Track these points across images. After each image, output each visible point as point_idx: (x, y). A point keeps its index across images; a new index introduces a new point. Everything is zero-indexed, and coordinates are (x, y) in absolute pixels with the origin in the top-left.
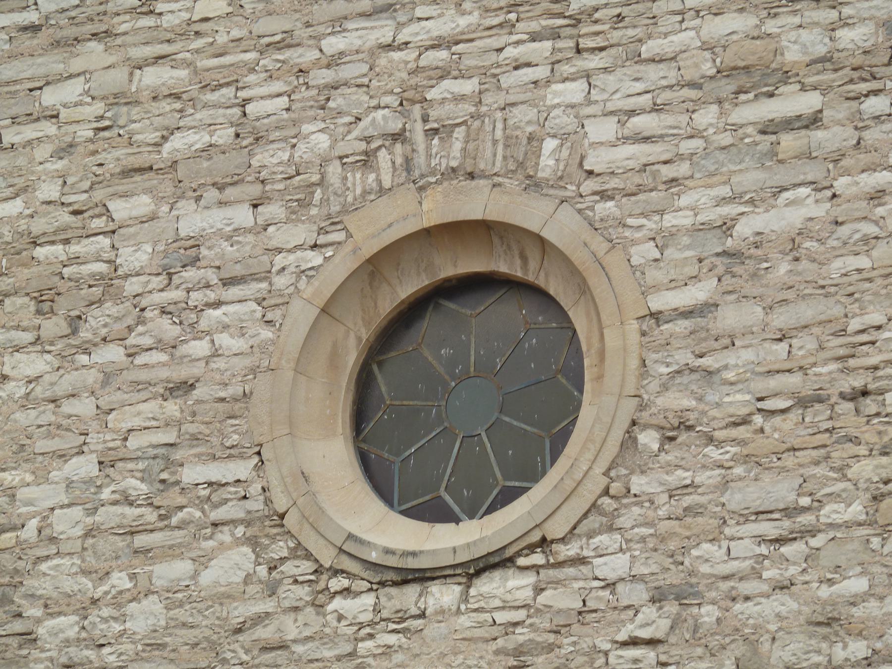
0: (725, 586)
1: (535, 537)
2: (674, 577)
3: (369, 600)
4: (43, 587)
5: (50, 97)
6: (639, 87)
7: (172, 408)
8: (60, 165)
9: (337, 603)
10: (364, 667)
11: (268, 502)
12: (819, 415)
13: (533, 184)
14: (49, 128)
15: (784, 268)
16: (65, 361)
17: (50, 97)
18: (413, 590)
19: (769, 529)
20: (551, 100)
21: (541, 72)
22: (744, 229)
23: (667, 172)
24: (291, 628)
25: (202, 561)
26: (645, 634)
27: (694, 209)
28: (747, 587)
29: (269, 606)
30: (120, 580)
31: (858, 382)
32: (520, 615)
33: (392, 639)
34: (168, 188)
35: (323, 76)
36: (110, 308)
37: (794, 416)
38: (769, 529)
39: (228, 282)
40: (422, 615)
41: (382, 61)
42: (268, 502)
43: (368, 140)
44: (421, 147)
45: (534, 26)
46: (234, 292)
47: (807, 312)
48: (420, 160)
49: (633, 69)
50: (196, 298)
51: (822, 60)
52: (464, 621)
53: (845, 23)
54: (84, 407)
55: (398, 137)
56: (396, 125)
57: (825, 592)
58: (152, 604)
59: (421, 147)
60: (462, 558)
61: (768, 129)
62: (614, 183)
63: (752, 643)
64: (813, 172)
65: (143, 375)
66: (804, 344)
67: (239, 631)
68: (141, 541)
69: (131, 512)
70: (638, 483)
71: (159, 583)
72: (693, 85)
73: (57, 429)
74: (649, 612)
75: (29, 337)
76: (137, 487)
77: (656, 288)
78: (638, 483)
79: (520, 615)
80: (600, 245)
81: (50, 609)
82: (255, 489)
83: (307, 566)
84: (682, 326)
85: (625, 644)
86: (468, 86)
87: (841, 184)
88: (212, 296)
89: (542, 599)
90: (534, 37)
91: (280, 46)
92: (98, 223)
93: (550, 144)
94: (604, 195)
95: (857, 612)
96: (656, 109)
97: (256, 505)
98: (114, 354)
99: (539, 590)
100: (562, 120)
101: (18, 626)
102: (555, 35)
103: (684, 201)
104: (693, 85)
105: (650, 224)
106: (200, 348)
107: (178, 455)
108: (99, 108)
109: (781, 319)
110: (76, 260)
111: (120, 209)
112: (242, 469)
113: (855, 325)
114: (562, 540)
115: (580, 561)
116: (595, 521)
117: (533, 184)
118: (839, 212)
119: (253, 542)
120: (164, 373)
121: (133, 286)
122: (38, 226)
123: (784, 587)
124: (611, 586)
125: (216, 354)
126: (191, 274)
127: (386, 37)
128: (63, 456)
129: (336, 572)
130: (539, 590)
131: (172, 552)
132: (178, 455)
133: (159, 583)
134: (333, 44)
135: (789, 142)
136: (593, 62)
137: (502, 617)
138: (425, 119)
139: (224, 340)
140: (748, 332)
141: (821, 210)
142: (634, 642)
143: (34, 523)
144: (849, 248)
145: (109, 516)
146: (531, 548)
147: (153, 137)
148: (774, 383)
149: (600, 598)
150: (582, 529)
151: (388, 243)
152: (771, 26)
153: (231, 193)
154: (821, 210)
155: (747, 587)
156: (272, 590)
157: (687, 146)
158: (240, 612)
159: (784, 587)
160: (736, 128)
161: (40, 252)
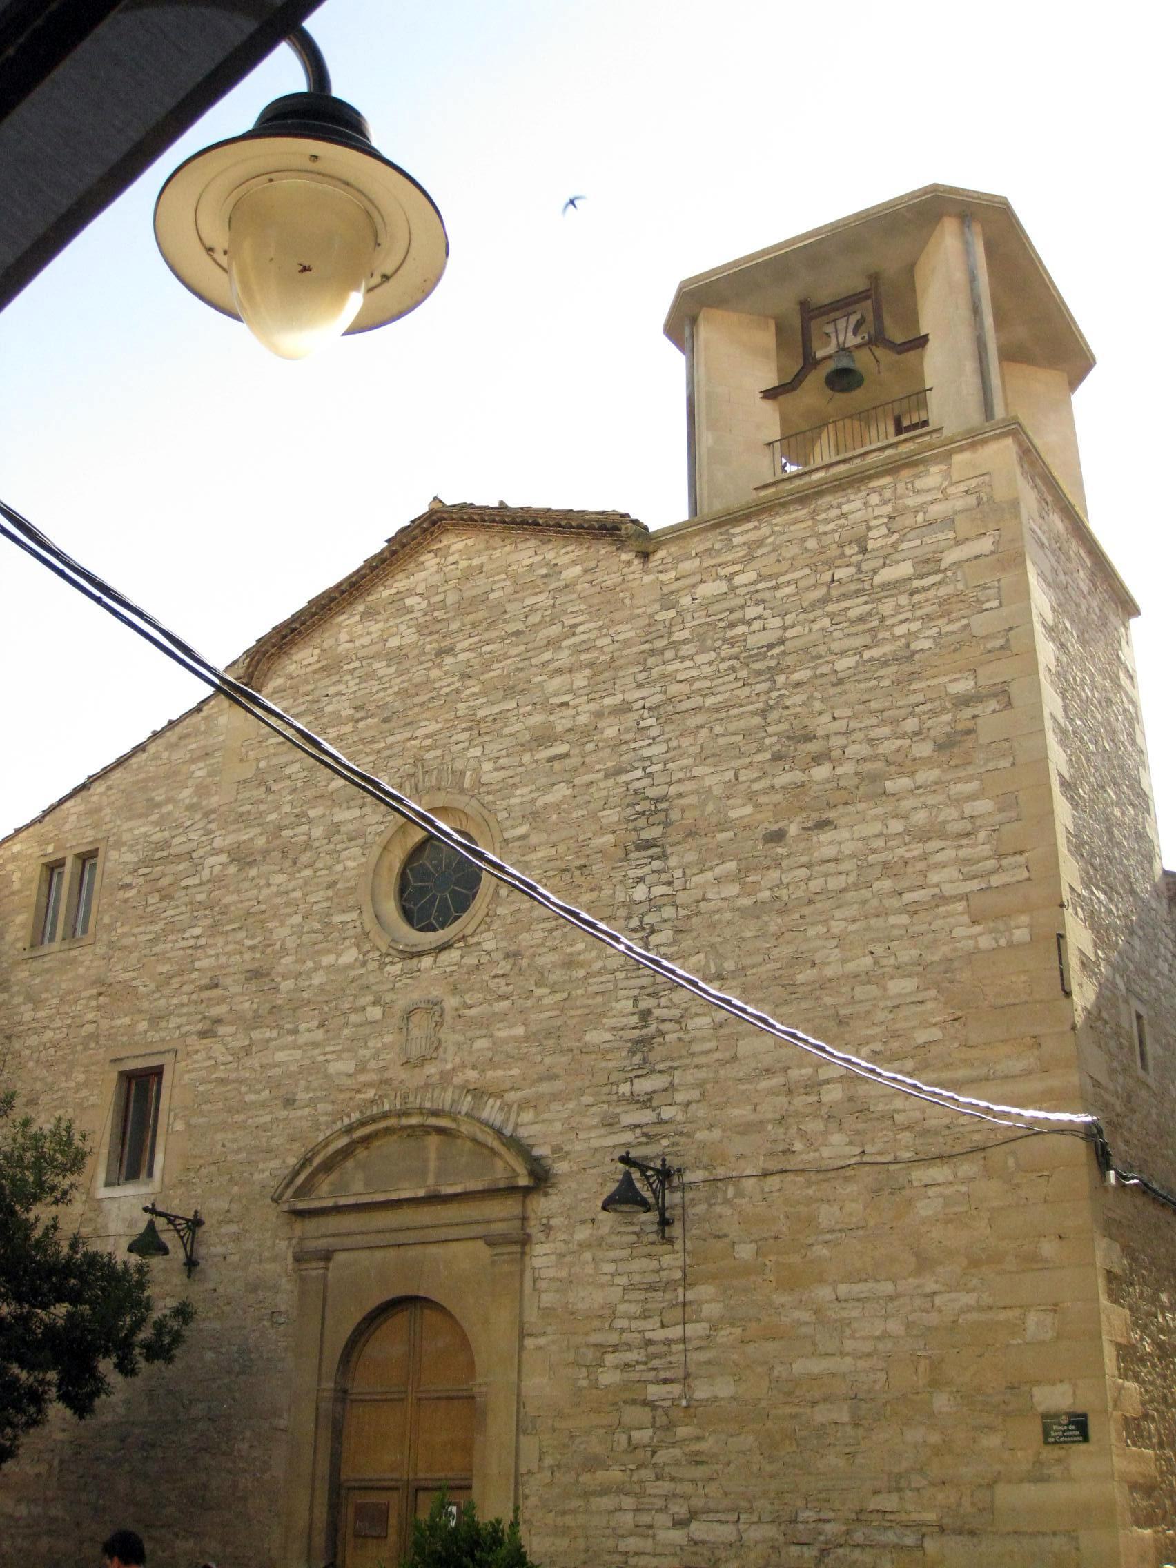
0: (531, 950)
1: (461, 935)
2: (513, 948)
3: (399, 965)
4: (280, 969)
5: (288, 771)
6: (501, 747)
7: (330, 893)
8: (290, 797)
9: (388, 968)
10: (715, 1565)
11: (363, 928)
12: (567, 876)
13: (462, 791)
14: (288, 782)
15: (555, 817)
16: (292, 876)
17: (288, 771)
18: (415, 960)
19: (548, 925)
20: (470, 755)
21: (465, 744)
22: (540, 803)
23: (511, 781)
24: (372, 979)
25: (339, 955)
26: (501, 972)
27: (522, 796)
28: (539, 951)
29: (363, 971)
30: (310, 964)
31: (582, 862)
32: (455, 968)
33: (409, 981)
34: (330, 803)
35: (386, 753)
36: (308, 854)
37: (558, 878)
38: (548, 925)
39: (350, 840)
40: (419, 970)
41: (408, 744)
42: (363, 928)
43: (401, 777)
44: (421, 778)
45: (464, 725)
46: (353, 843)
47: (564, 834)
48: (420, 785)
49: (500, 740)
50: (339, 847)
51: (569, 730)
52: (434, 972)
53: (578, 714)
54: (298, 894)
55: (413, 775)
56: (412, 771)
57: (569, 950)
58: (321, 973)
59: (421, 778)
60: (434, 945)
61: (550, 760)
62: (493, 787)
63: (542, 974)
64: (566, 776)
65: (320, 880)
66: (562, 848)
67: (352, 981)
68: (316, 947)
69: (314, 935)
70: (500, 911)
71: (324, 964)
72: (522, 745)
73: (287, 904)
74: (503, 963)
75: (277, 868)
76: (317, 926)
77: (506, 830)
78: (500, 911)
79: (455, 968)
80: (485, 813)
81: (284, 978)
82: (358, 924)
83: (377, 953)
84: (517, 844)
85: (494, 977)
86: (439, 752)
87: (577, 781)
88: (344, 846)
89: (464, 961)
90: (464, 730)
91: (371, 742)
92: (304, 820)
93: (468, 773)
94: (488, 793)
95: (582, 957)
96: (508, 756)
97: (359, 930)
98: (307, 873)
99: (462, 957)
100: (472, 763)
101: (273, 985)
102: (471, 729)
103: (518, 792)
104: (522, 745)
105: (505, 803)
106: (339, 867)
107: (332, 911)
108: (305, 774)
109: (554, 838)
110: (295, 835)
111: (312, 813)
112: (354, 915)
113: (581, 838)
114: (472, 936)
115: (478, 944)
116: (483, 927)
117: (462, 791)
118: (576, 791)
119: (358, 946)
120: (327, 879)
121: (316, 844)
122: (284, 823)
123: (554, 949)
124: (489, 953)
125: (345, 869)
126: (338, 837)
127: (408, 735)
128: (290, 915)
129: (389, 955)
130: (462, 957)
131: (329, 951)
132: (332, 911)
133: (324, 964)
134: (390, 740)
135: (557, 765)
136: (486, 738)
137: (448, 969)
138: (423, 767)
139: (350, 864)
140: (541, 844)
141: (568, 792)
142: (496, 976)
143: (279, 943)
144: (578, 807)
145: (305, 938)
146: (459, 941)
147: (324, 783)
148: (552, 864)
149: (484, 959)
150: (479, 930)
151: (65, 71)
152: (551, 718)
153: (352, 803)
154: (568, 792)
155: (539, 951)
156: (364, 964)
157: (520, 769)
158: (353, 974)
159: (554, 949)
160: (537, 762)
161: (284, 833)
